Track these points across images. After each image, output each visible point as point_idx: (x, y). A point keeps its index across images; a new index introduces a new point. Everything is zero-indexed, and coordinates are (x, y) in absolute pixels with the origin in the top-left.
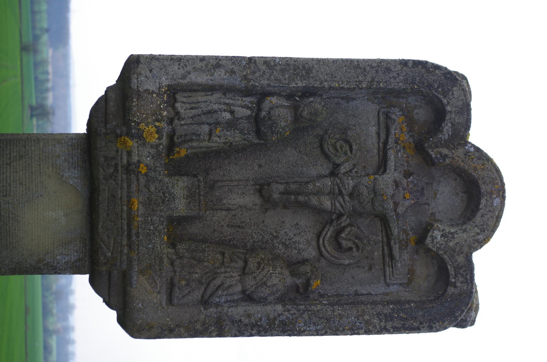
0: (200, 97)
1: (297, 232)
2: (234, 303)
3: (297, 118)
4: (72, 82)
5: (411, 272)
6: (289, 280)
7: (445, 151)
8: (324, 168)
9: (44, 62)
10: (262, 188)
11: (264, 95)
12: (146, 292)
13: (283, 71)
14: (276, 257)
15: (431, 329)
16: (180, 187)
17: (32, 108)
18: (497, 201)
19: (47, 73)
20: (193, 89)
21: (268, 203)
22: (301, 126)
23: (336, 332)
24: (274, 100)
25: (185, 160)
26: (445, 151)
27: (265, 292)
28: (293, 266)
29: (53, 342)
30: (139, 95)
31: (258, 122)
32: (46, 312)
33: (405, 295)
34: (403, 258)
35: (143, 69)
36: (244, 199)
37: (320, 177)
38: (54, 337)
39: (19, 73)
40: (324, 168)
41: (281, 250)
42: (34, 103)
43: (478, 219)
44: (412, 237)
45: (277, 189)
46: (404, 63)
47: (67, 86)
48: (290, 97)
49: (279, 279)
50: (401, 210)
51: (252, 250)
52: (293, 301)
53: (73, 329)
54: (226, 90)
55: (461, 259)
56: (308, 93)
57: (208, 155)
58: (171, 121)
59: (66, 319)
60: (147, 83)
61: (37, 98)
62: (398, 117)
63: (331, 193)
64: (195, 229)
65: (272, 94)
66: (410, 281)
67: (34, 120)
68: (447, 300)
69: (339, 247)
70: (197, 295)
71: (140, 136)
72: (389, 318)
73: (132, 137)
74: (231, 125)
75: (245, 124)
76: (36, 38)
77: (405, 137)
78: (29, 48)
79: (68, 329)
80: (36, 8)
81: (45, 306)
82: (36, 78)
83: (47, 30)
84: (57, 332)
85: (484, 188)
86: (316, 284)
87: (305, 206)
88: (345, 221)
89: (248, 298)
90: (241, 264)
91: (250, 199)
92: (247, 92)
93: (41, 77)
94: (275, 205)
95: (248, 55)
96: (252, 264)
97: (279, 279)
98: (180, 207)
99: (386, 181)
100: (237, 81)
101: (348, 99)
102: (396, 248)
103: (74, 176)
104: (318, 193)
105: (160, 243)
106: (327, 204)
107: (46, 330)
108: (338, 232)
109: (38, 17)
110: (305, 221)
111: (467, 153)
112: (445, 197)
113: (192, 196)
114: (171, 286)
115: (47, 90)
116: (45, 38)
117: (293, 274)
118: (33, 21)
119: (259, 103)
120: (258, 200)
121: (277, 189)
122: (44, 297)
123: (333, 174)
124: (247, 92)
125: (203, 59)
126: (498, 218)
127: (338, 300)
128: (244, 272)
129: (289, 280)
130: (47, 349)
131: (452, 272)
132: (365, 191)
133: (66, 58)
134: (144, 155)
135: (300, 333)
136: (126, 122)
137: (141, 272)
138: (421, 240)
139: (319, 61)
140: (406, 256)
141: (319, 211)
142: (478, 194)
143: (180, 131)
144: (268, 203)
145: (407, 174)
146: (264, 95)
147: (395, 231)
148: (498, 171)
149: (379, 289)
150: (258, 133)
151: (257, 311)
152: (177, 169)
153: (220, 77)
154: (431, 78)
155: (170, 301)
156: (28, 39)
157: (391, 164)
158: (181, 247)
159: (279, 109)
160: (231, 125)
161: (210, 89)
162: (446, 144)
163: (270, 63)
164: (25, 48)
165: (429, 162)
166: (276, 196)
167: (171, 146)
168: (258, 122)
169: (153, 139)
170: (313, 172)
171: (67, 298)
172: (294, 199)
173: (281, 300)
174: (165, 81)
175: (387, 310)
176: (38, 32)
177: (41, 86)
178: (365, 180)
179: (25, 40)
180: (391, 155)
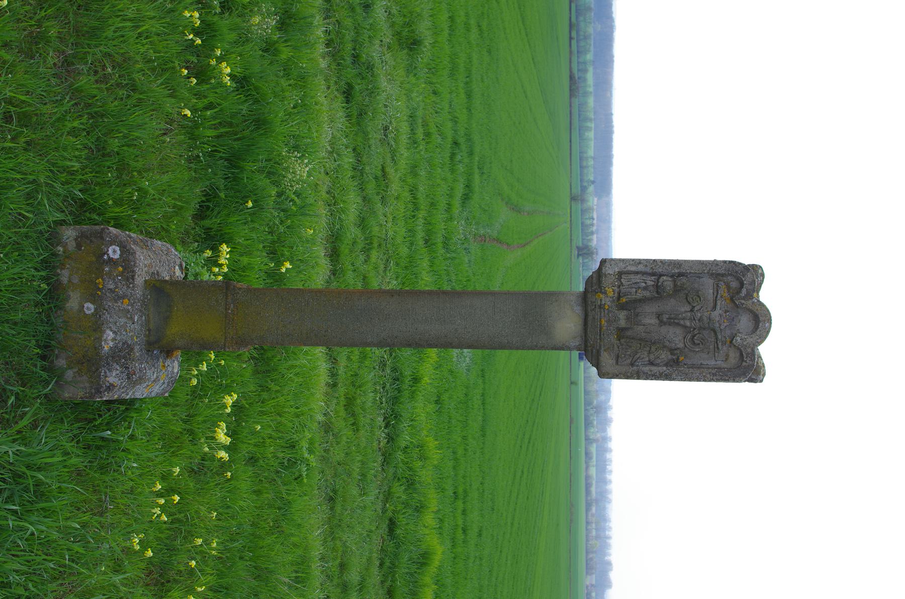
0: (632, 276)
1: (675, 336)
2: (645, 365)
3: (675, 285)
4: (613, 226)
5: (727, 356)
6: (670, 357)
7: (743, 301)
8: (688, 308)
9: (590, 209)
10: (659, 316)
11: (661, 275)
12: (607, 359)
13: (669, 265)
14: (665, 347)
15: (734, 381)
16: (622, 315)
17: (578, 248)
18: (767, 325)
19: (593, 219)
20: (629, 273)
21: (662, 323)
22: (677, 290)
23: (690, 380)
24: (665, 278)
25: (628, 305)
26: (743, 301)
27: (658, 361)
28: (672, 351)
29: (593, 449)
30: (606, 276)
31: (658, 287)
32: (588, 423)
33: (724, 365)
34: (724, 349)
35: (607, 264)
36: (651, 321)
37: (686, 312)
38: (594, 445)
39: (569, 219)
40: (688, 308)
41: (667, 344)
42: (580, 245)
43: (758, 332)
44: (728, 340)
45: (665, 318)
46: (725, 262)
47: (609, 229)
48: (672, 276)
49: (665, 356)
50: (722, 327)
51: (654, 343)
52: (671, 366)
53: (610, 439)
54: (643, 273)
55: (749, 350)
56: (681, 275)
57: (636, 301)
58: (619, 287)
59: (604, 430)
60: (609, 270)
61: (583, 239)
62: (722, 286)
63: (690, 319)
64: (629, 333)
65: (664, 275)
66: (726, 359)
67: (581, 258)
68: (747, 369)
69: (694, 343)
70: (629, 361)
71: (605, 293)
72: (714, 375)
73: (602, 293)
74: (645, 288)
75: (651, 288)
76: (584, 189)
77: (726, 294)
78: (577, 198)
79: (606, 439)
80: (585, 164)
81: (587, 418)
82: (582, 223)
83: (593, 182)
84: (596, 441)
85: (761, 319)
86: (681, 358)
87: (678, 324)
88: (696, 332)
89: (651, 363)
90: (648, 349)
91: (654, 321)
92: (653, 274)
93: (588, 222)
94: (665, 324)
95: (653, 258)
96: (653, 349)
97: (665, 356)
98: (623, 323)
99: (715, 315)
100: (648, 270)
101: (700, 277)
102: (720, 344)
103: (578, 309)
104: (684, 319)
105: (613, 338)
106: (688, 324)
107: (587, 439)
108: (694, 336)
109: (585, 171)
110: (679, 331)
111: (753, 303)
112: (744, 322)
113: (628, 318)
114: (618, 357)
115: (592, 233)
116: (591, 188)
117: (672, 354)
118: (581, 174)
119: (658, 280)
120: (657, 322)
121: (665, 318)
122: (586, 410)
123: (692, 311)
124: (653, 274)
125: (633, 260)
126: (768, 332)
127: (693, 366)
128: (649, 352)
129: (670, 357)
130: (588, 454)
131: (745, 356)
132: (705, 319)
133: (608, 205)
134: (607, 299)
135: (674, 380)
136: (600, 287)
137: (605, 350)
138: (731, 342)
139: (685, 261)
140: (725, 348)
141: (685, 327)
142: (760, 321)
143: (623, 291)
144: (662, 323)
145: (726, 312)
146: (661, 275)
147: (720, 337)
148: (768, 311)
149: (712, 363)
150: (658, 292)
151: (655, 369)
152: (622, 307)
153: (641, 268)
154: (737, 269)
155: (617, 363)
156: (576, 190)
157: (718, 307)
158: (623, 341)
159: (667, 283)
160: (645, 288)
161: (637, 273)
162: (744, 298)
163: (662, 262)
164: (573, 198)
165: (737, 306)
166: (665, 320)
167: (619, 298)
168: (658, 287)
169: (611, 294)
170: (683, 310)
171: (606, 412)
172: (673, 321)
173: (666, 365)
174: (617, 270)
175: (714, 371)
176: (585, 184)
177: (586, 230)
178: (706, 314)
179: (574, 191)
180: (719, 303)
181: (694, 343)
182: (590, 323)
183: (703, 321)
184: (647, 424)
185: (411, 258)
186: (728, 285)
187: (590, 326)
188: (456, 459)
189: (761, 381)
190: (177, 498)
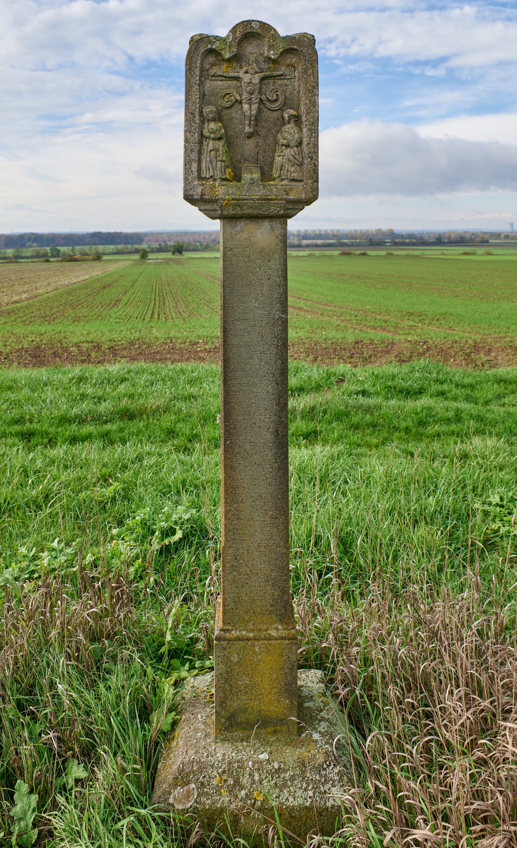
0: (203, 165)
11: (202, 135)
16: (246, 176)
48: (203, 122)
65: (202, 132)
69: (276, 100)
88: (263, 97)
103: (240, 225)
112: (251, 49)
115: (166, 245)
146: (202, 135)
152: (237, 178)
153: (194, 156)
157: (236, 74)
181: (276, 100)
182: (256, 212)
183: (250, 103)
184: (358, 173)
185: (500, 381)
186: (213, 65)
187: (261, 212)
189: (313, 36)
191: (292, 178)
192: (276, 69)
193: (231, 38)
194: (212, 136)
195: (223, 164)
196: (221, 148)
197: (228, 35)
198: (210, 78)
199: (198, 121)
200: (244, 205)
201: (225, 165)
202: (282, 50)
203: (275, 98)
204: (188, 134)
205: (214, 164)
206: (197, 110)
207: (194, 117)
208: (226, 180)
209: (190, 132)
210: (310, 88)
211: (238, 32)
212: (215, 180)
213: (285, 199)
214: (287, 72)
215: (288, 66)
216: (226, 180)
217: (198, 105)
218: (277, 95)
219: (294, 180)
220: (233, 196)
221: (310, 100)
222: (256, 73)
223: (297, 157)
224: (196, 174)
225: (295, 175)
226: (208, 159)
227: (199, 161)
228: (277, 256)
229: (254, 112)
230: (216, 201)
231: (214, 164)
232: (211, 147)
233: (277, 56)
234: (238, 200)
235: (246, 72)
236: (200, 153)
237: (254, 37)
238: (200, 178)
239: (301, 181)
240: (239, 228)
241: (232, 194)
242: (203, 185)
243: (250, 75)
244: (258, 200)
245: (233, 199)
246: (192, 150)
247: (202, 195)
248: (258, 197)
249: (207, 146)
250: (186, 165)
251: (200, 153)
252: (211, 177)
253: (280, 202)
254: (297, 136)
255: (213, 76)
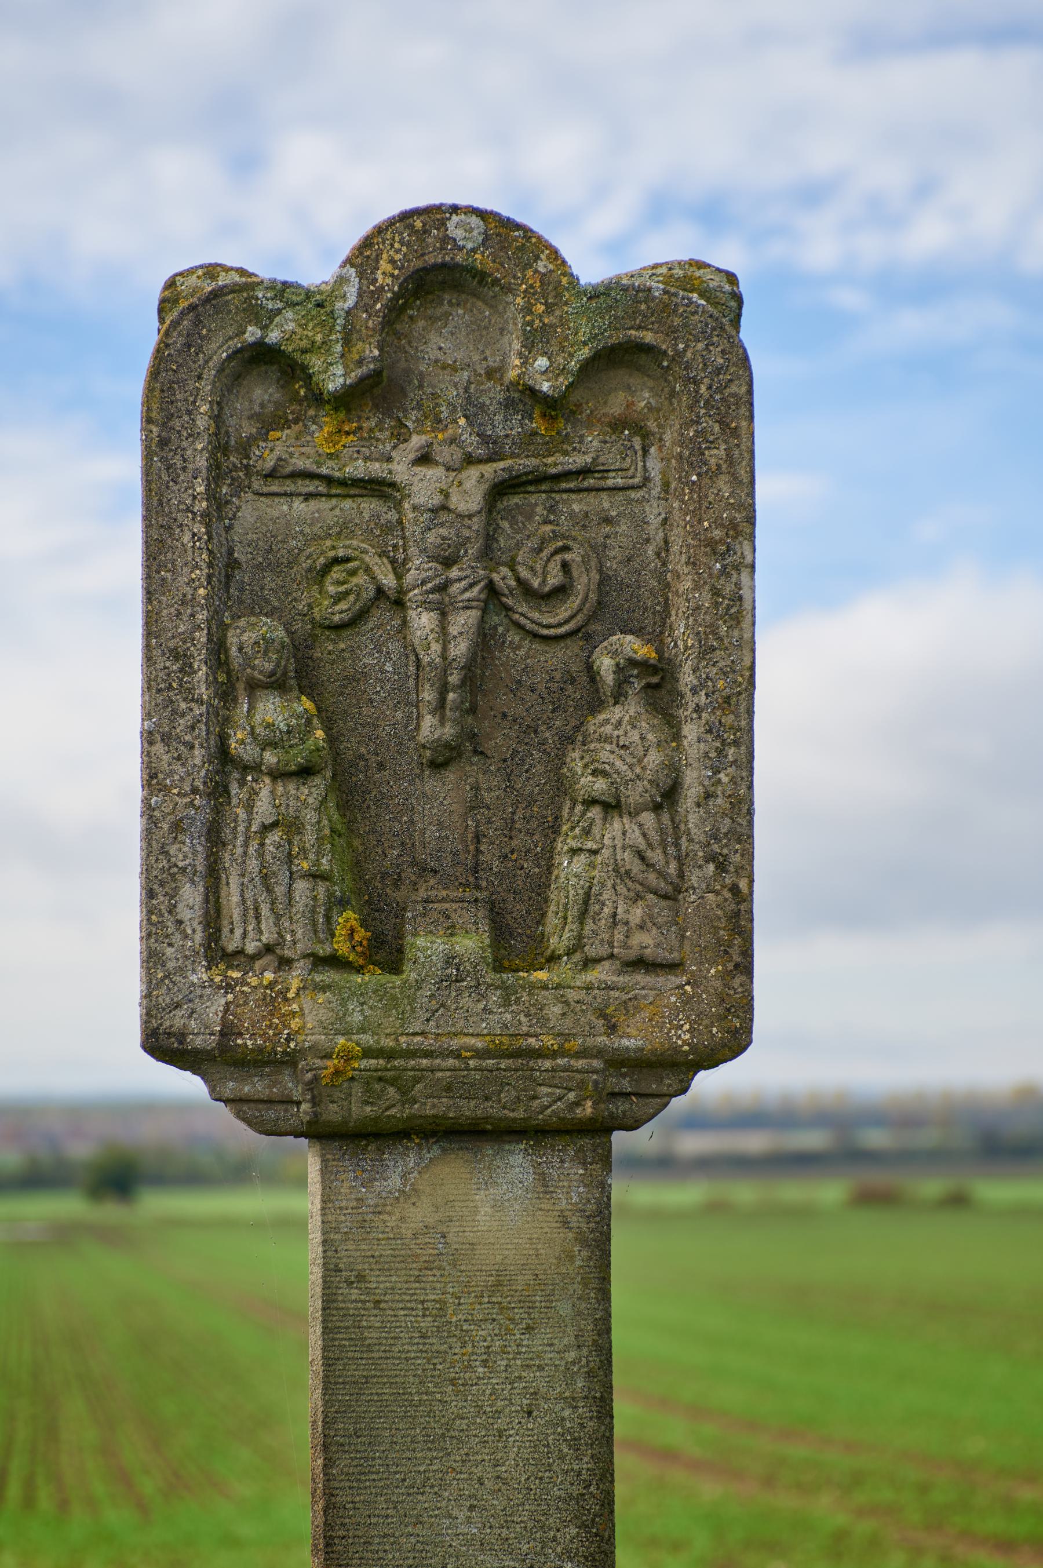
0: (232, 896)
3: (277, 684)
11: (223, 756)
16: (427, 947)
65: (223, 739)
69: (561, 591)
88: (502, 577)
103: (400, 1168)
108: (526, 590)
142: (443, 267)
146: (223, 756)
157: (376, 469)
180: (357, 469)
181: (561, 591)
182: (471, 1109)
186: (270, 423)
187: (492, 1109)
188: (370, 1327)
190: (665, 364)
191: (632, 954)
192: (559, 444)
193: (351, 292)
194: (270, 758)
195: (321, 888)
196: (310, 816)
197: (341, 280)
198: (257, 484)
199: (203, 691)
200: (417, 1080)
201: (330, 895)
202: (585, 352)
203: (554, 579)
204: (159, 748)
205: (280, 890)
206: (202, 636)
207: (187, 669)
208: (334, 961)
209: (167, 739)
210: (717, 533)
211: (384, 265)
212: (285, 963)
213: (599, 1053)
214: (611, 459)
215: (617, 425)
216: (334, 961)
217: (202, 616)
218: (565, 566)
219: (640, 964)
220: (368, 1039)
221: (716, 592)
222: (470, 460)
223: (656, 856)
224: (199, 937)
225: (645, 942)
226: (253, 864)
227: (213, 877)
228: (565, 1309)
229: (460, 649)
230: (290, 1060)
231: (280, 890)
232: (264, 809)
233: (563, 382)
234: (390, 1054)
235: (424, 459)
236: (215, 837)
237: (457, 287)
238: (215, 953)
239: (673, 967)
240: (395, 1181)
241: (362, 1030)
242: (229, 988)
243: (439, 472)
244: (481, 1054)
245: (368, 1053)
246: (177, 827)
247: (228, 1031)
248: (479, 1043)
249: (249, 807)
250: (150, 894)
251: (215, 837)
252: (268, 949)
253: (580, 1064)
254: (654, 759)
255: (271, 475)
